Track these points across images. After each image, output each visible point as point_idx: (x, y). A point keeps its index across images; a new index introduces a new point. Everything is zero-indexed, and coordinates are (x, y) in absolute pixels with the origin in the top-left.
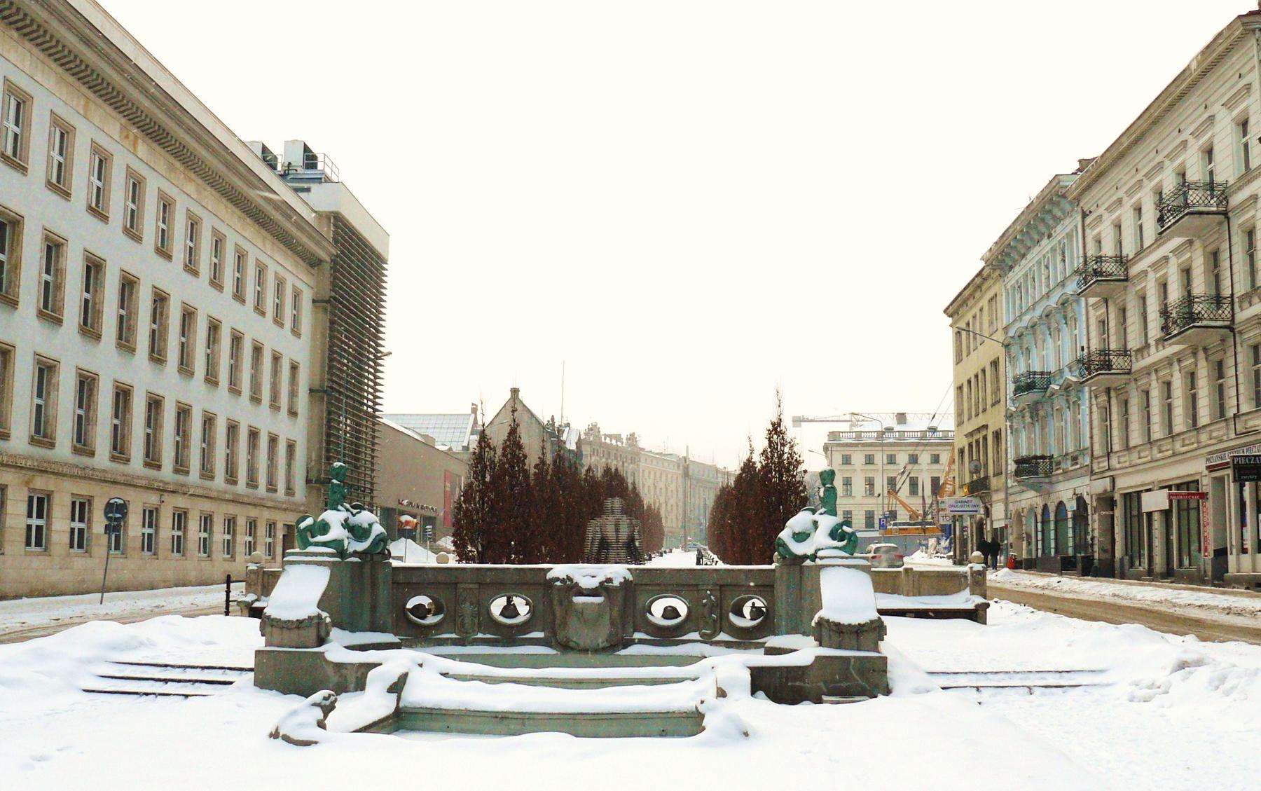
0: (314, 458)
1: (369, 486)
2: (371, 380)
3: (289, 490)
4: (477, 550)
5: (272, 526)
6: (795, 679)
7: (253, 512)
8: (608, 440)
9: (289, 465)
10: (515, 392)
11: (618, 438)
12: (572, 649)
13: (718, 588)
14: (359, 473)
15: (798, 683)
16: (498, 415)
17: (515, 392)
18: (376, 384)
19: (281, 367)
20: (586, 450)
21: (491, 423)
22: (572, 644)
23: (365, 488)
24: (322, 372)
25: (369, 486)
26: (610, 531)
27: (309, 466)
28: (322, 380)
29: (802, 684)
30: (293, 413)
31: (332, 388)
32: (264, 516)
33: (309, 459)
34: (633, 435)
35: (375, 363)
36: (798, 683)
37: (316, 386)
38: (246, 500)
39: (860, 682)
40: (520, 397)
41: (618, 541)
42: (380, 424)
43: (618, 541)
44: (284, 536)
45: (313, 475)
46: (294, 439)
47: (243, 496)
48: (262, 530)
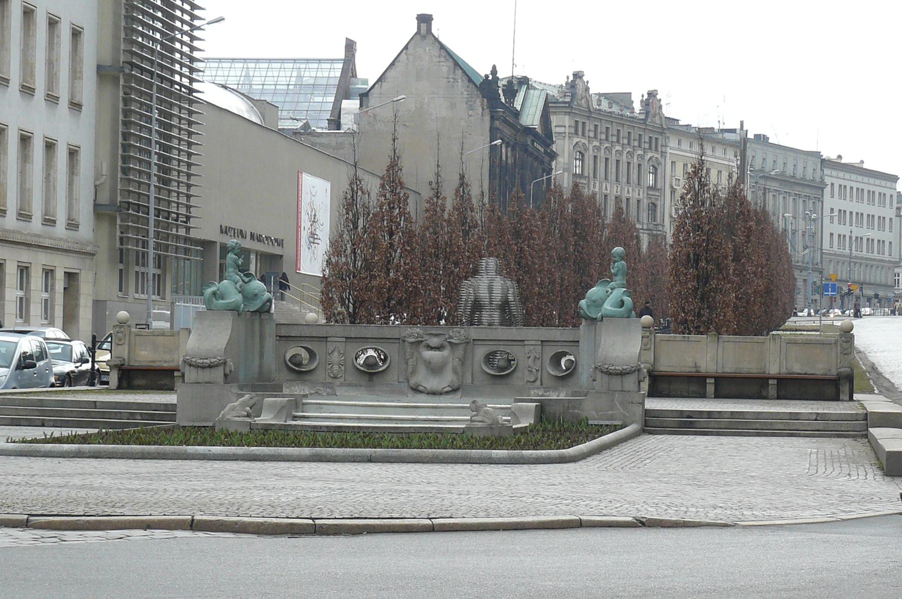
0: (104, 171)
1: (183, 211)
2: (186, 33)
3: (72, 225)
4: (348, 310)
5: (49, 273)
6: (574, 408)
7: (25, 256)
8: (605, 106)
9: (71, 184)
10: (425, 20)
11: (623, 99)
12: (421, 392)
13: (540, 342)
14: (170, 191)
15: (576, 411)
16: (393, 64)
17: (425, 20)
18: (193, 38)
19: (59, 37)
20: (560, 123)
21: (380, 80)
22: (421, 388)
23: (178, 214)
24: (116, 37)
25: (183, 211)
26: (484, 293)
27: (98, 183)
28: (116, 50)
29: (579, 412)
30: (75, 106)
31: (133, 65)
32: (38, 261)
33: (98, 175)
34: (652, 94)
35: (191, 25)
36: (576, 411)
37: (107, 61)
38: (18, 238)
39: (622, 410)
40: (434, 31)
41: (491, 303)
42: (198, 102)
43: (491, 303)
44: (65, 288)
45: (104, 198)
46: (77, 144)
47: (13, 232)
48: (37, 280)
